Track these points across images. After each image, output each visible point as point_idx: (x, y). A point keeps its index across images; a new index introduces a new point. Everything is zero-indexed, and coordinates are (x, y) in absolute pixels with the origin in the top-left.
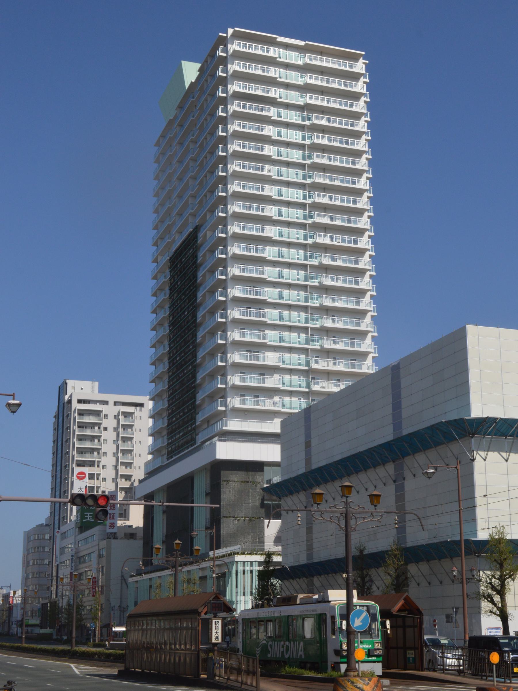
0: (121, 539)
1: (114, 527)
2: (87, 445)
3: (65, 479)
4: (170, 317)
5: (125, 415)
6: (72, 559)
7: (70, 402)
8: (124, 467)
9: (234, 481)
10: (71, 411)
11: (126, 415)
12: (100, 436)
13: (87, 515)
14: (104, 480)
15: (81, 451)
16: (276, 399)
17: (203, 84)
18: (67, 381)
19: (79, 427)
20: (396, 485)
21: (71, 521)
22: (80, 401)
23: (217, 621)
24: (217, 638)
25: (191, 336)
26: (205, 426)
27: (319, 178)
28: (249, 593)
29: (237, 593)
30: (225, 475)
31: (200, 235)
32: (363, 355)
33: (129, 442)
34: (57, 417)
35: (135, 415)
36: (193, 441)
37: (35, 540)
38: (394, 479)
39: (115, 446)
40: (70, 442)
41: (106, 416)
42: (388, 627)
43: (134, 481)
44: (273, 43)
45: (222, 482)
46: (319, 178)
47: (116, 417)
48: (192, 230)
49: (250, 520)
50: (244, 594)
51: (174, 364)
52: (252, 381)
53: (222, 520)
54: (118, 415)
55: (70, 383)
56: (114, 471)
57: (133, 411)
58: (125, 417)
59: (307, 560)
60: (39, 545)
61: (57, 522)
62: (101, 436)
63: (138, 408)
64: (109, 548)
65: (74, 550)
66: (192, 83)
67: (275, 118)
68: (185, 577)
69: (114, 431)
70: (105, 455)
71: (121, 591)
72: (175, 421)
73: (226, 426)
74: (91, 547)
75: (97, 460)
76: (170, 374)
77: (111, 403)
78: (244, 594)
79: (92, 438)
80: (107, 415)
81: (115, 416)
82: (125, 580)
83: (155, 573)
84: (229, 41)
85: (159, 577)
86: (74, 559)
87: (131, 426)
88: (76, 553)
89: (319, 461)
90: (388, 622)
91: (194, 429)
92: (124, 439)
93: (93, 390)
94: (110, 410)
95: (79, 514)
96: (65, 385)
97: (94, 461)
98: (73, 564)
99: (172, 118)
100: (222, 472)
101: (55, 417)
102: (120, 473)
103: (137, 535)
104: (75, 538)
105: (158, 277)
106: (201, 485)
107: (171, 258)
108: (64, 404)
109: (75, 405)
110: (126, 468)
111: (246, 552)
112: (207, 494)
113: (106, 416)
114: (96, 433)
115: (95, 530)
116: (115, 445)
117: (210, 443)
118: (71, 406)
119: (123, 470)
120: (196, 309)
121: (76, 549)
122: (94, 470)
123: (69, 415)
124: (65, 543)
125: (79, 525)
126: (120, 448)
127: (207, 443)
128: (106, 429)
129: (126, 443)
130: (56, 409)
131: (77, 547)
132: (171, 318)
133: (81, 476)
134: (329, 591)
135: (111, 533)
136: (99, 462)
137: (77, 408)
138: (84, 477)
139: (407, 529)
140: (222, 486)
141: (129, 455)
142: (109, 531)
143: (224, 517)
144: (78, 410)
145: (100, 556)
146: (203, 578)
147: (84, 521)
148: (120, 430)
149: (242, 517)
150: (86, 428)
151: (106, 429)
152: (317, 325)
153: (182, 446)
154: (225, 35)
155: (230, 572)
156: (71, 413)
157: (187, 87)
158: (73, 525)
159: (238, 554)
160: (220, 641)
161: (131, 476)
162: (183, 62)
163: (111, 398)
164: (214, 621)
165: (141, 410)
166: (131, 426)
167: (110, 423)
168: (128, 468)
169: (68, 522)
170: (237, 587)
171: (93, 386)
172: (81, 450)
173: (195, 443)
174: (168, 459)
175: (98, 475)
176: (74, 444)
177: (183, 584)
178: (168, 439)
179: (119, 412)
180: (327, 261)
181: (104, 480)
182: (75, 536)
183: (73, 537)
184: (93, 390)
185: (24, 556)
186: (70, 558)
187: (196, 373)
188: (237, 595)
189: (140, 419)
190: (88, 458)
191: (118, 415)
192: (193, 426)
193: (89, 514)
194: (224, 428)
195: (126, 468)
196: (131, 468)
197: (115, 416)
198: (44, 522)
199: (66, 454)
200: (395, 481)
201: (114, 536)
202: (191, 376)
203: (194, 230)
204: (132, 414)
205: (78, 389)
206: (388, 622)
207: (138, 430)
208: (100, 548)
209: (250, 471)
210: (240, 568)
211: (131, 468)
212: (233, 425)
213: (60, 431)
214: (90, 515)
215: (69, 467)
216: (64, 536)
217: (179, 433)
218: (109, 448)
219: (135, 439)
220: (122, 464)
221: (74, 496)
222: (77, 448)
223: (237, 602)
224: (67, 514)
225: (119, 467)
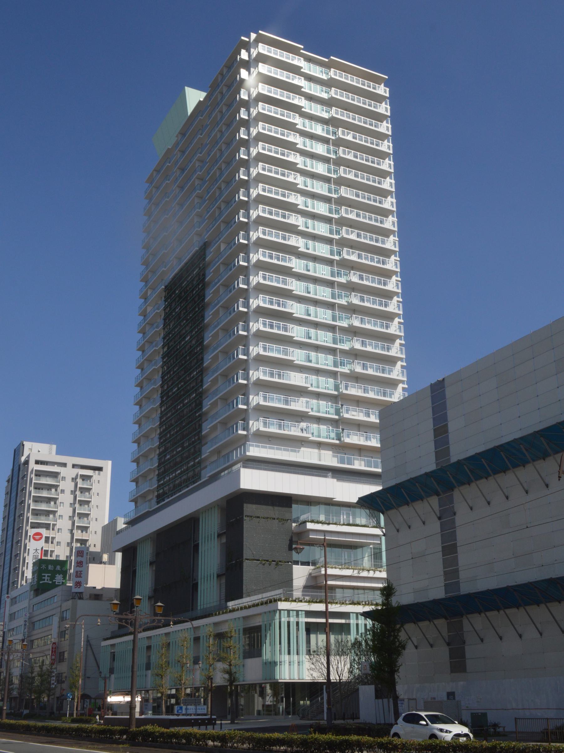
0: (87, 599)
1: (80, 586)
2: (43, 507)
5: (84, 478)
6: (25, 625)
7: (27, 462)
8: (80, 531)
9: (258, 517)
10: (27, 471)
11: (85, 478)
12: (57, 499)
13: (45, 576)
15: (36, 513)
16: (303, 425)
18: (24, 443)
19: (35, 488)
21: (21, 585)
22: (37, 462)
25: (195, 361)
27: (345, 192)
28: (305, 652)
29: (280, 650)
30: (249, 509)
33: (86, 506)
34: (10, 481)
35: (94, 478)
36: (197, 476)
38: (439, 516)
39: (71, 509)
43: (90, 546)
45: (245, 518)
46: (345, 192)
47: (74, 480)
48: (198, 249)
49: (277, 564)
50: (289, 653)
52: (276, 402)
53: (245, 564)
54: (76, 478)
55: (28, 445)
56: (69, 535)
57: (92, 474)
58: (83, 480)
59: (446, 594)
62: (57, 499)
63: (97, 472)
65: (28, 615)
66: (200, 102)
68: (211, 630)
69: (72, 494)
70: (61, 518)
74: (51, 610)
75: (52, 523)
76: (163, 409)
77: (69, 466)
78: (289, 653)
80: (65, 477)
81: (73, 479)
83: (154, 631)
84: (252, 46)
85: (147, 637)
87: (89, 490)
88: (30, 618)
89: (459, 451)
91: (199, 463)
94: (68, 473)
95: (36, 575)
97: (49, 524)
98: (26, 630)
99: (170, 147)
100: (245, 505)
101: (8, 481)
102: (75, 538)
106: (211, 526)
108: (20, 465)
109: (32, 466)
110: (82, 532)
112: (151, 563)
114: (53, 495)
116: (72, 509)
117: (229, 473)
118: (28, 467)
119: (78, 535)
121: (30, 613)
123: (25, 476)
124: (15, 608)
125: (36, 587)
126: (77, 511)
127: (223, 474)
129: (82, 507)
130: (9, 473)
131: (31, 611)
135: (76, 593)
136: (54, 525)
137: (35, 469)
141: (86, 519)
143: (247, 559)
144: (36, 471)
145: (62, 619)
147: (41, 582)
148: (78, 493)
149: (267, 561)
150: (42, 489)
152: (346, 346)
153: (180, 484)
154: (247, 40)
155: (269, 626)
156: (27, 474)
157: (189, 114)
159: (280, 600)
161: (87, 540)
162: (186, 88)
163: (70, 460)
165: (99, 474)
167: (67, 485)
168: (84, 532)
169: (19, 587)
170: (280, 643)
171: (51, 449)
173: (200, 479)
174: (158, 503)
176: (29, 505)
177: (209, 639)
178: (159, 481)
179: (77, 475)
180: (355, 279)
182: (30, 600)
183: (27, 601)
188: (280, 653)
189: (99, 483)
190: (42, 520)
191: (76, 478)
192: (197, 461)
193: (46, 575)
195: (82, 532)
196: (87, 532)
197: (73, 479)
199: (19, 516)
200: (440, 518)
201: (80, 596)
202: (194, 404)
204: (90, 477)
205: (35, 451)
208: (63, 610)
210: (284, 620)
211: (87, 532)
214: (48, 576)
215: (22, 530)
216: (14, 601)
217: (176, 470)
220: (78, 527)
222: (33, 509)
225: (75, 531)
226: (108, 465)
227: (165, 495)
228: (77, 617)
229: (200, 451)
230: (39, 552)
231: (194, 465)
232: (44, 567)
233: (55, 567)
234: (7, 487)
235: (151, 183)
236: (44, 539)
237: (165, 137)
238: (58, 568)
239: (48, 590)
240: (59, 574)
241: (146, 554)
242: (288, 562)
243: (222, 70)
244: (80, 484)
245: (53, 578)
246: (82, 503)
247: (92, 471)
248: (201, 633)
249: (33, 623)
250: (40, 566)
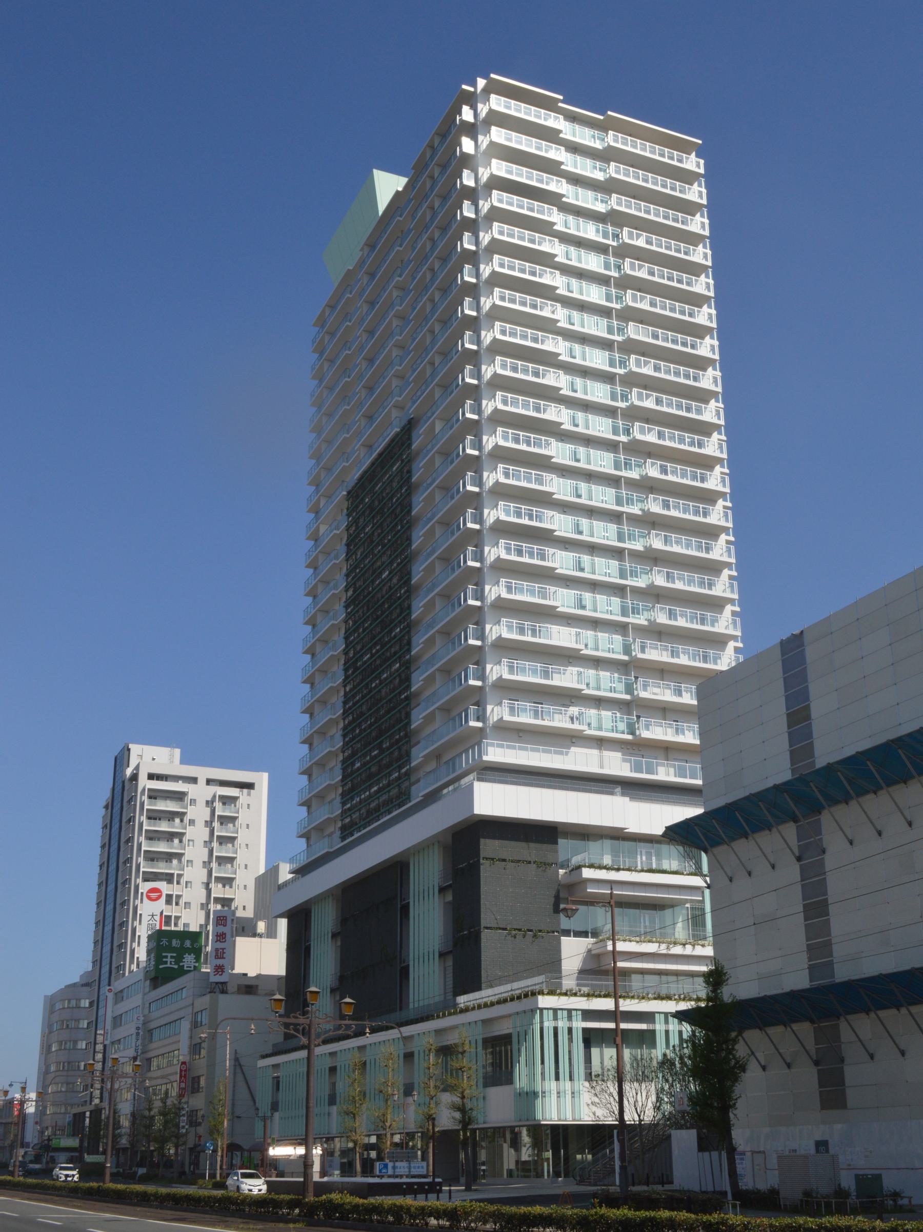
1: (223, 971)
3: (123, 903)
4: (347, 591)
6: (138, 1034)
7: (135, 777)
8: (220, 886)
9: (504, 860)
10: (136, 791)
11: (227, 801)
12: (183, 834)
13: (166, 957)
14: (188, 905)
15: (152, 857)
16: (574, 710)
18: (131, 746)
19: (149, 818)
20: (801, 866)
21: (131, 972)
22: (151, 777)
26: (432, 765)
29: (543, 1074)
30: (489, 847)
32: (719, 641)
33: (230, 845)
34: (110, 806)
36: (404, 796)
37: (64, 1008)
38: (797, 855)
40: (133, 842)
41: (193, 802)
47: (210, 803)
48: (398, 430)
49: (535, 936)
50: (557, 1078)
51: (356, 669)
52: (529, 674)
54: (213, 801)
56: (204, 892)
58: (224, 804)
59: (811, 981)
60: (72, 1019)
61: (105, 976)
63: (245, 791)
64: (213, 1009)
66: (397, 192)
69: (206, 826)
71: (234, 1087)
72: (359, 769)
75: (176, 872)
77: (202, 781)
78: (557, 1078)
81: (207, 802)
82: (240, 1065)
86: (141, 1033)
87: (233, 819)
88: (144, 1024)
91: (407, 774)
92: (223, 840)
94: (200, 793)
95: (153, 955)
96: (126, 753)
97: (172, 875)
98: (139, 1042)
100: (482, 841)
101: (106, 807)
102: (213, 895)
103: (260, 988)
104: (143, 998)
106: (428, 875)
107: (349, 493)
108: (123, 782)
109: (144, 783)
110: (224, 886)
111: (558, 991)
112: (334, 936)
113: (193, 802)
117: (455, 790)
118: (137, 785)
119: (218, 891)
120: (409, 561)
122: (174, 890)
123: (132, 799)
124: (122, 1007)
125: (153, 975)
126: (215, 854)
127: (445, 791)
128: (192, 822)
129: (224, 846)
130: (107, 794)
132: (350, 593)
133: (154, 895)
135: (217, 983)
137: (148, 787)
139: (835, 948)
140: (482, 867)
141: (229, 866)
144: (149, 790)
145: (195, 1025)
147: (161, 967)
148: (216, 824)
150: (160, 819)
151: (192, 822)
153: (377, 809)
154: (472, 89)
156: (136, 796)
157: (380, 213)
158: (141, 976)
159: (541, 993)
161: (232, 900)
162: (375, 171)
163: (203, 773)
165: (249, 794)
166: (233, 819)
167: (198, 813)
168: (227, 887)
169: (127, 974)
170: (543, 1062)
172: (151, 856)
173: (409, 799)
174: (343, 838)
175: (179, 897)
177: (429, 1055)
178: (344, 804)
179: (214, 796)
181: (188, 905)
182: (144, 994)
183: (140, 996)
185: (43, 1036)
186: (134, 1031)
187: (411, 674)
188: (543, 1079)
191: (213, 801)
192: (404, 770)
193: (169, 955)
194: (485, 758)
195: (224, 886)
196: (231, 887)
197: (207, 802)
198: (76, 979)
199: (125, 863)
200: (799, 859)
201: (222, 988)
203: (403, 429)
205: (147, 758)
207: (244, 826)
208: (195, 1010)
209: (532, 841)
210: (548, 1024)
211: (231, 887)
212: (496, 753)
214: (172, 957)
216: (119, 996)
217: (371, 786)
218: (195, 852)
219: (239, 841)
220: (218, 879)
222: (145, 852)
223: (544, 1092)
224: (125, 960)
225: (212, 885)
226: (262, 780)
227: (355, 824)
229: (408, 754)
230: (158, 918)
231: (399, 778)
232: (164, 942)
233: (182, 944)
235: (323, 326)
236: (163, 898)
237: (343, 252)
240: (190, 954)
241: (325, 921)
242: (553, 932)
244: (220, 810)
245: (179, 959)
246: (223, 840)
247: (238, 790)
248: (415, 1047)
249: (150, 1032)
250: (159, 941)
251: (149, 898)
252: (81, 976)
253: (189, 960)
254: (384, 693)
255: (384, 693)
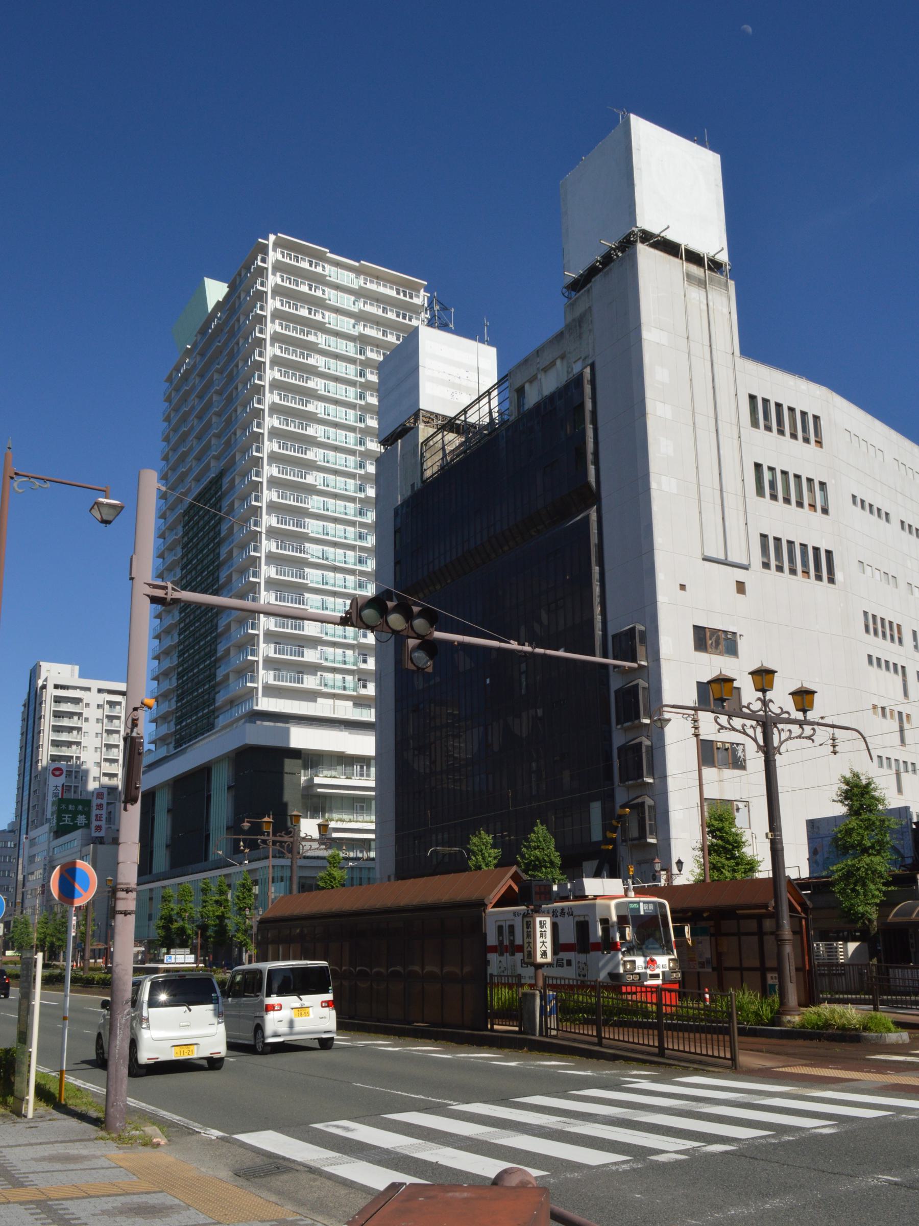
11: (112, 704)
17: (234, 302)
18: (41, 663)
22: (56, 687)
23: (543, 919)
24: (544, 954)
31: (226, 482)
34: (27, 705)
41: (87, 705)
42: (688, 935)
44: (322, 258)
50: (361, 878)
66: (218, 302)
67: (322, 346)
73: (257, 705)
79: (70, 729)
90: (687, 929)
91: (213, 711)
93: (72, 675)
101: (24, 705)
105: (167, 534)
109: (51, 692)
112: (229, 788)
113: (87, 705)
115: (77, 835)
124: (35, 850)
130: (25, 696)
131: (51, 854)
133: (57, 773)
134: (584, 880)
138: (61, 774)
142: (95, 834)
146: (205, 891)
157: (210, 310)
160: (549, 959)
162: (206, 279)
163: (95, 684)
164: (538, 920)
171: (73, 671)
174: (176, 748)
184: (72, 675)
194: (256, 708)
206: (687, 929)
213: (31, 722)
220: (106, 760)
221: (360, 603)
228: (415, 668)
229: (214, 699)
230: (60, 789)
231: (208, 713)
232: (63, 807)
233: (76, 807)
234: (23, 713)
238: (80, 808)
239: (70, 832)
241: (163, 802)
243: (240, 271)
244: (107, 710)
245: (74, 819)
246: (109, 732)
250: (59, 806)
251: (54, 775)
252: (9, 825)
253: (81, 819)
254: (199, 661)
255: (199, 661)
